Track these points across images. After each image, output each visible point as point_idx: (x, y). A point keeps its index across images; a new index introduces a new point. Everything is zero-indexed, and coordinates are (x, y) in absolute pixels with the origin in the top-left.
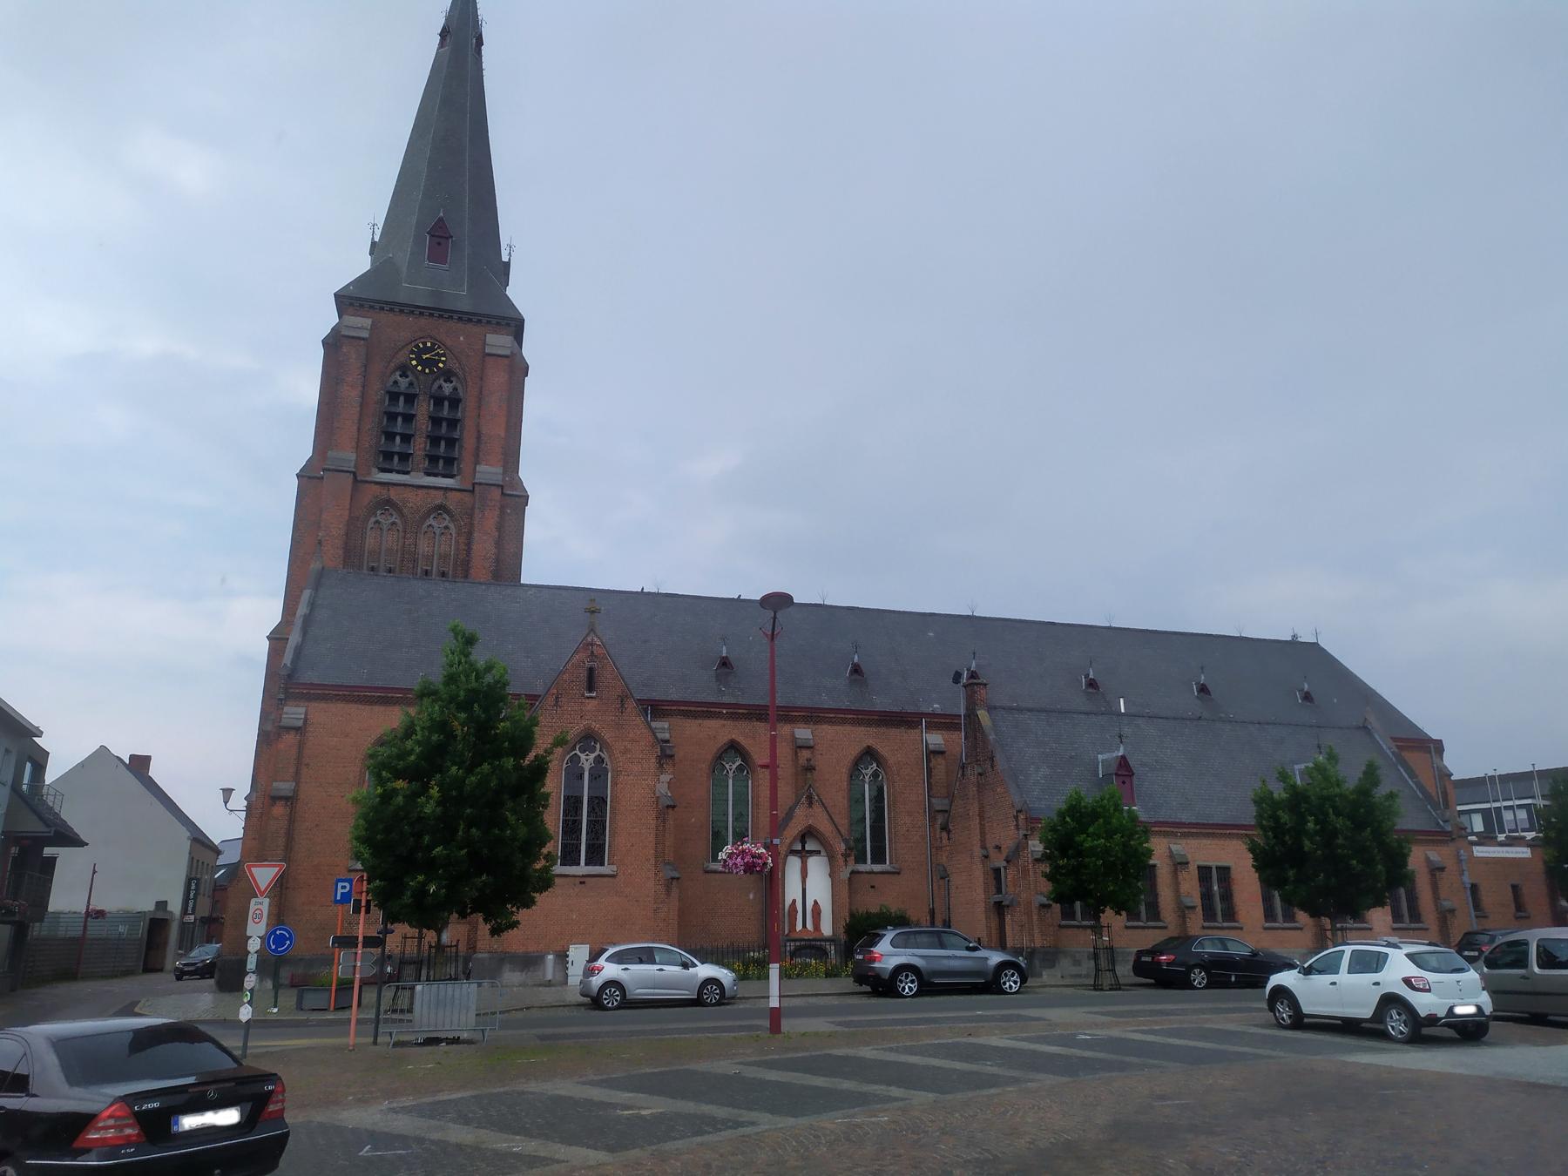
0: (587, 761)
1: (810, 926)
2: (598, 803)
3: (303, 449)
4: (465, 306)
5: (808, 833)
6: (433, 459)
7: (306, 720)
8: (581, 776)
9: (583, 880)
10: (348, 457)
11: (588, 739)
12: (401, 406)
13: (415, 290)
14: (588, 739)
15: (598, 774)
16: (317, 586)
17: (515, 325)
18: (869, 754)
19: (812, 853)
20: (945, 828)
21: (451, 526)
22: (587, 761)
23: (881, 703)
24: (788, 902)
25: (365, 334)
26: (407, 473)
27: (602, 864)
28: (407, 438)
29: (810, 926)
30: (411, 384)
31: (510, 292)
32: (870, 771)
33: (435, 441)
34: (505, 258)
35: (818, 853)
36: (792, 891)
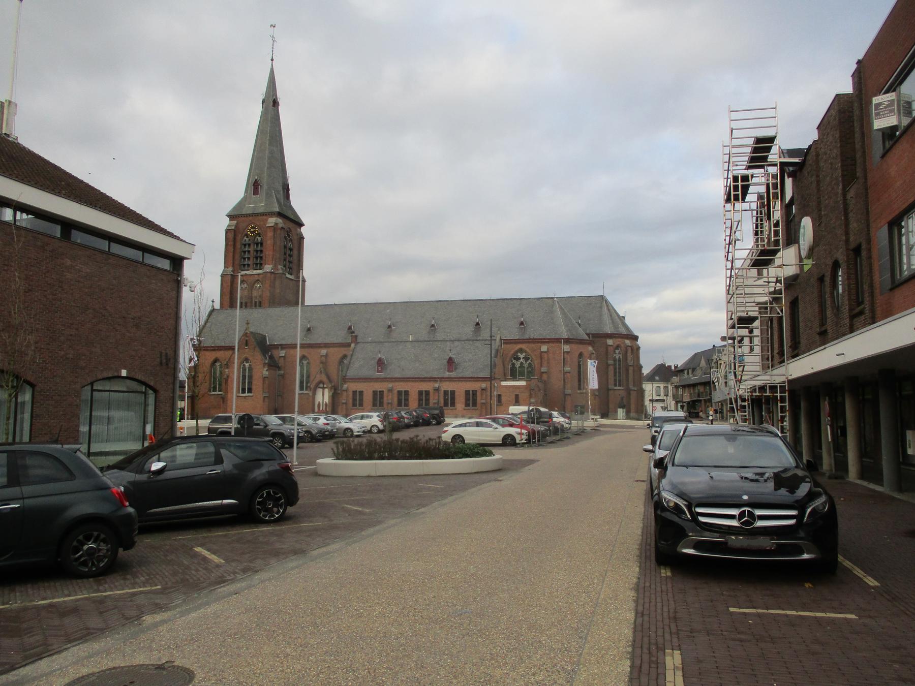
2: (250, 377)
6: (257, 264)
11: (247, 360)
13: (248, 209)
15: (250, 369)
22: (247, 365)
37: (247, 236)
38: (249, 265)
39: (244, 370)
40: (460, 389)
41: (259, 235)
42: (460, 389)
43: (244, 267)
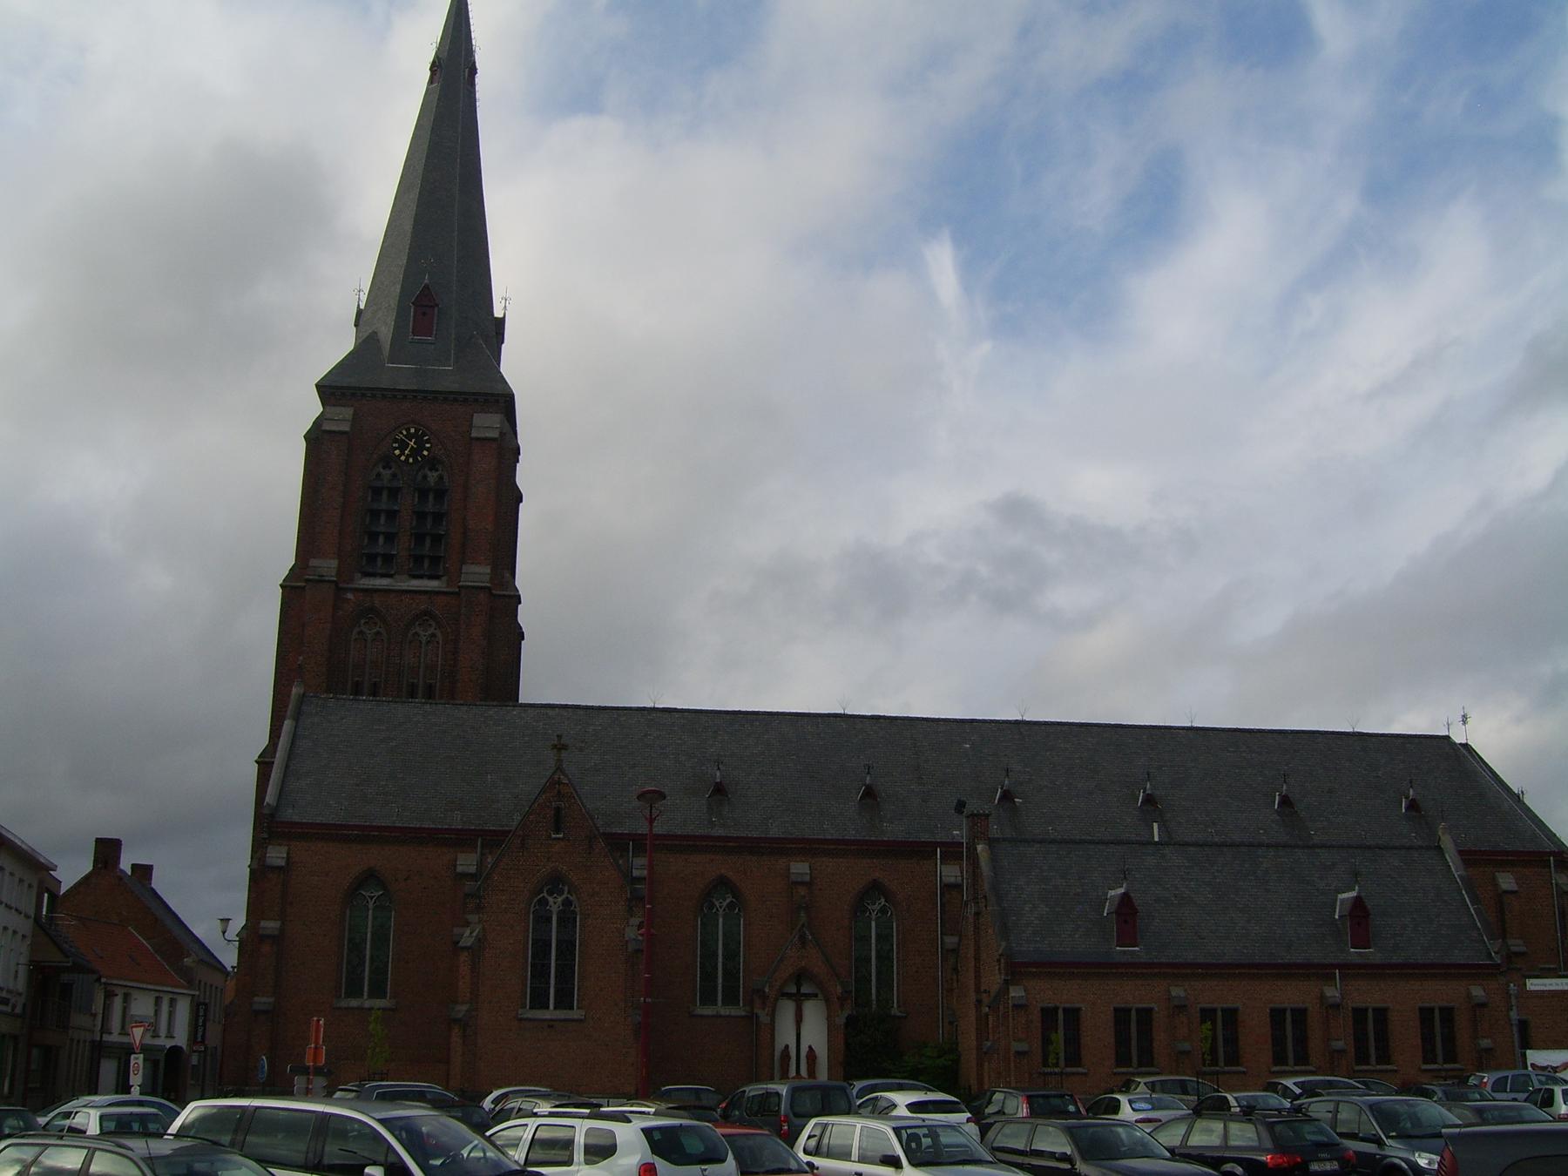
0: (555, 904)
1: (804, 1072)
2: (566, 948)
3: (286, 558)
4: (451, 384)
5: (800, 977)
6: (418, 560)
7: (288, 858)
8: (549, 920)
9: (551, 1024)
10: (328, 566)
11: (555, 882)
12: (382, 525)
13: (398, 374)
14: (555, 882)
15: (567, 919)
16: (297, 718)
17: (505, 403)
18: (875, 888)
19: (808, 996)
20: (955, 969)
21: (438, 632)
22: (555, 904)
23: (894, 830)
24: (779, 1047)
25: (346, 427)
26: (391, 576)
27: (571, 1008)
28: (390, 538)
29: (804, 1072)
30: (394, 475)
31: (504, 369)
32: (877, 907)
33: (419, 538)
34: (498, 313)
35: (816, 996)
36: (785, 1035)
37: (388, 461)
38: (388, 559)
39: (543, 919)
40: (1402, 1001)
41: (432, 463)
42: (1402, 1001)
43: (373, 563)
